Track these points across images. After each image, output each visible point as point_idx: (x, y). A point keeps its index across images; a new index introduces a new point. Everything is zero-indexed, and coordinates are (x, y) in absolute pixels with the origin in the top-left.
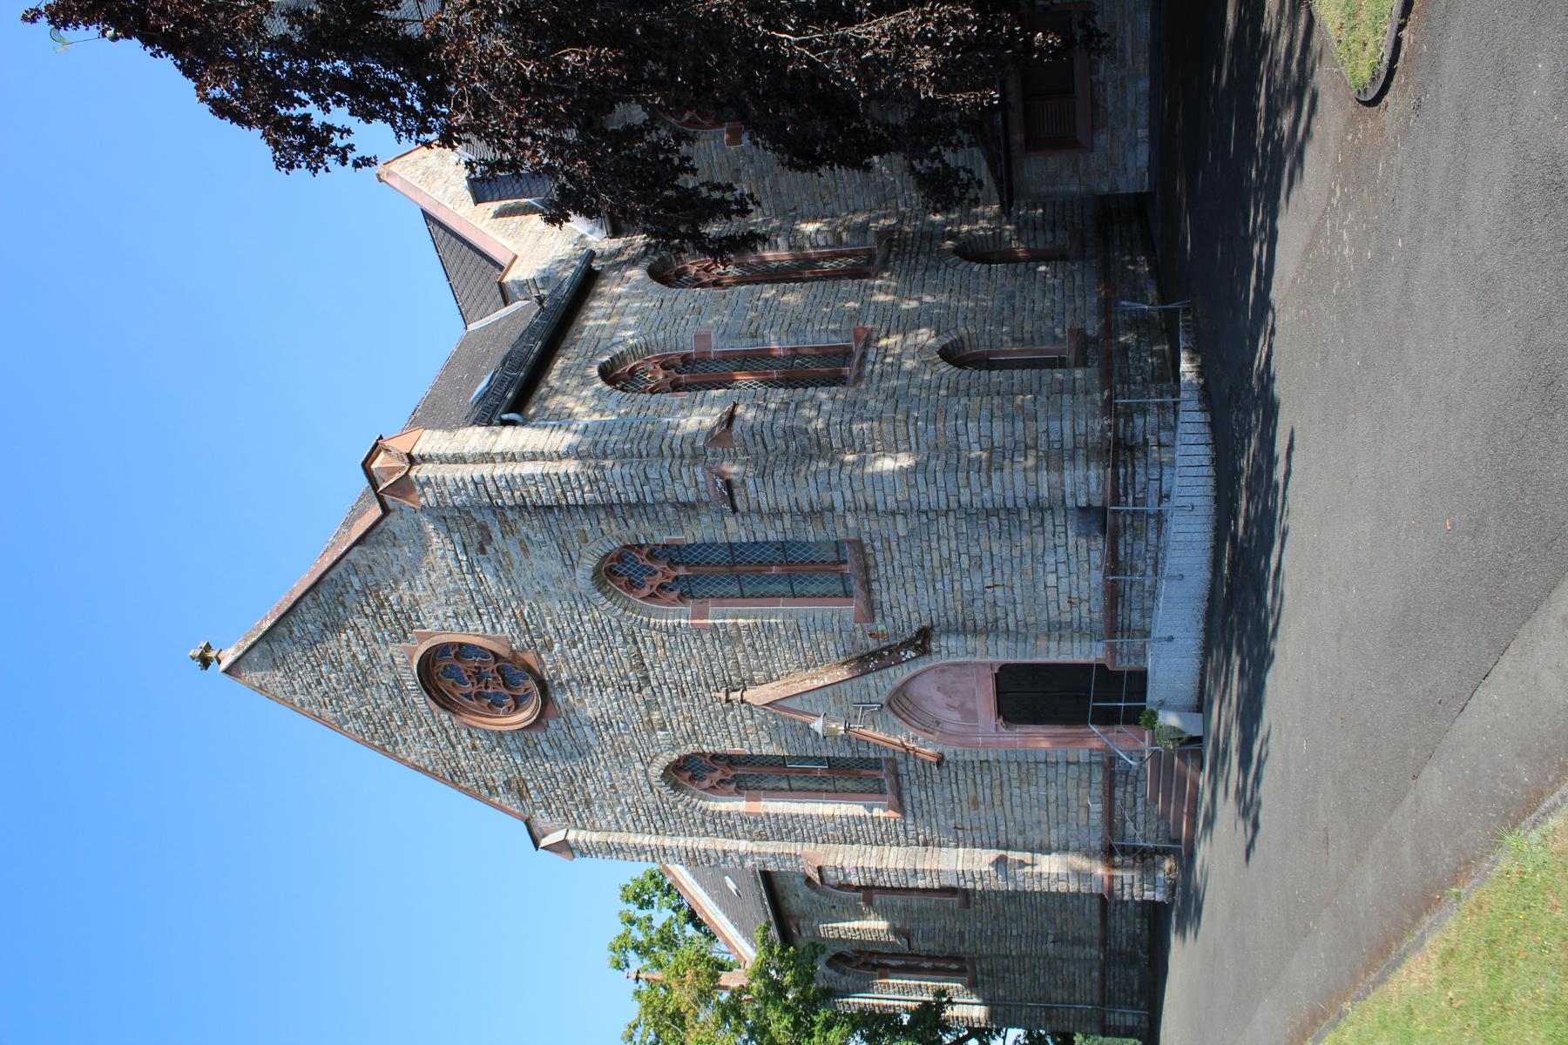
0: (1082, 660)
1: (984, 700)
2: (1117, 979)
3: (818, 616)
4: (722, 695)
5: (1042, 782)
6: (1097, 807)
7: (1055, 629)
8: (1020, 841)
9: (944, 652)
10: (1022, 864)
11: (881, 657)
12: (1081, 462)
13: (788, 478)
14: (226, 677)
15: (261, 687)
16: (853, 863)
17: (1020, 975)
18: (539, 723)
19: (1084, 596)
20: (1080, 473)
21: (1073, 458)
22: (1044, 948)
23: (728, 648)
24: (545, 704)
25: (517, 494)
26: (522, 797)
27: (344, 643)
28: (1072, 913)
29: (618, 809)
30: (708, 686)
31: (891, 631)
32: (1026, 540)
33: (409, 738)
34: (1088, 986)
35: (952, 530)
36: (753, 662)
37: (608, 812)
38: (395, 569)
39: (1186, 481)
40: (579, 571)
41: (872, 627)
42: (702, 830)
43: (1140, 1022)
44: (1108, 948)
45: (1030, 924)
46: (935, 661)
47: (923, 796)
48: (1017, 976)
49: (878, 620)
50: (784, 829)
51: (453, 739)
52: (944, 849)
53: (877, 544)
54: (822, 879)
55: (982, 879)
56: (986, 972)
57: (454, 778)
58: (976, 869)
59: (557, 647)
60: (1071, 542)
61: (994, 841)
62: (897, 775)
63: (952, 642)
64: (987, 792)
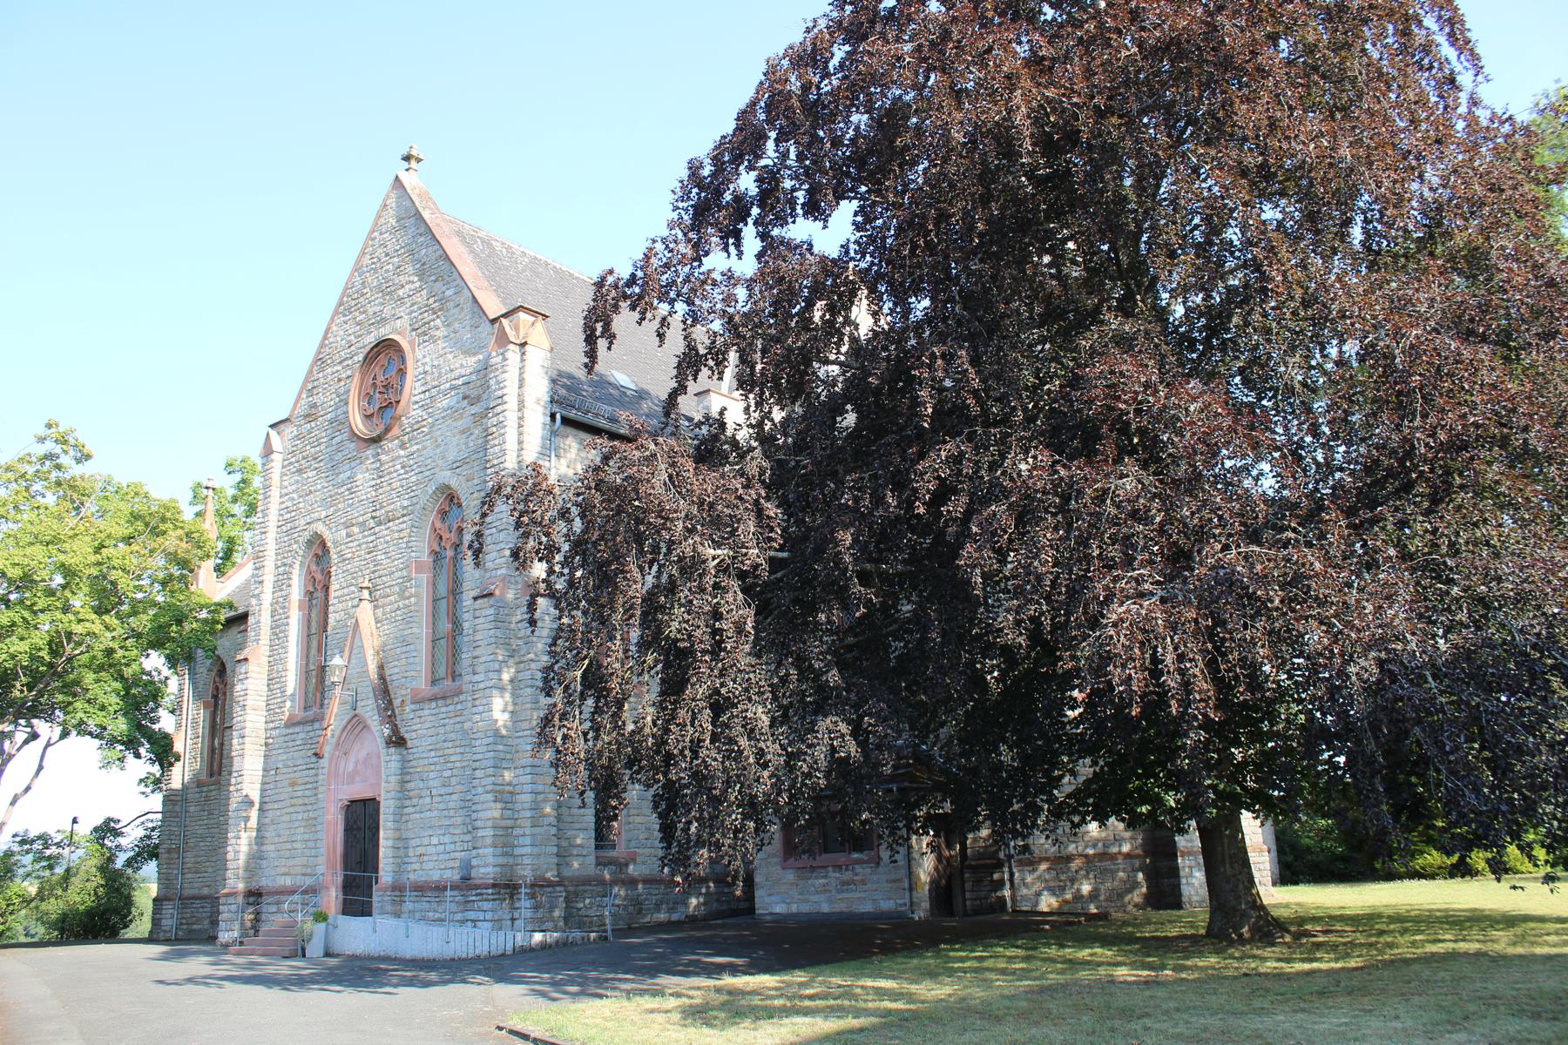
0: (381, 866)
1: (360, 791)
3: (417, 660)
4: (366, 584)
5: (306, 837)
6: (288, 881)
7: (402, 843)
8: (267, 821)
9: (388, 758)
10: (247, 819)
11: (386, 709)
12: (501, 860)
13: (493, 640)
14: (393, 178)
15: (385, 205)
16: (250, 687)
18: (354, 436)
19: (425, 866)
20: (491, 860)
21: (504, 854)
23: (397, 588)
24: (365, 440)
25: (494, 429)
26: (306, 416)
27: (412, 278)
29: (295, 496)
30: (374, 572)
31: (405, 716)
32: (459, 820)
33: (347, 327)
34: (196, 885)
36: (388, 609)
37: (294, 487)
38: (457, 325)
39: (465, 936)
40: (449, 473)
41: (408, 702)
42: (279, 563)
46: (383, 751)
47: (298, 743)
49: (413, 707)
50: (278, 629)
51: (346, 363)
52: (262, 759)
53: (459, 707)
54: (239, 661)
55: (237, 790)
57: (319, 361)
58: (244, 786)
59: (402, 453)
60: (458, 855)
61: (267, 799)
62: (312, 721)
63: (394, 765)
64: (300, 793)
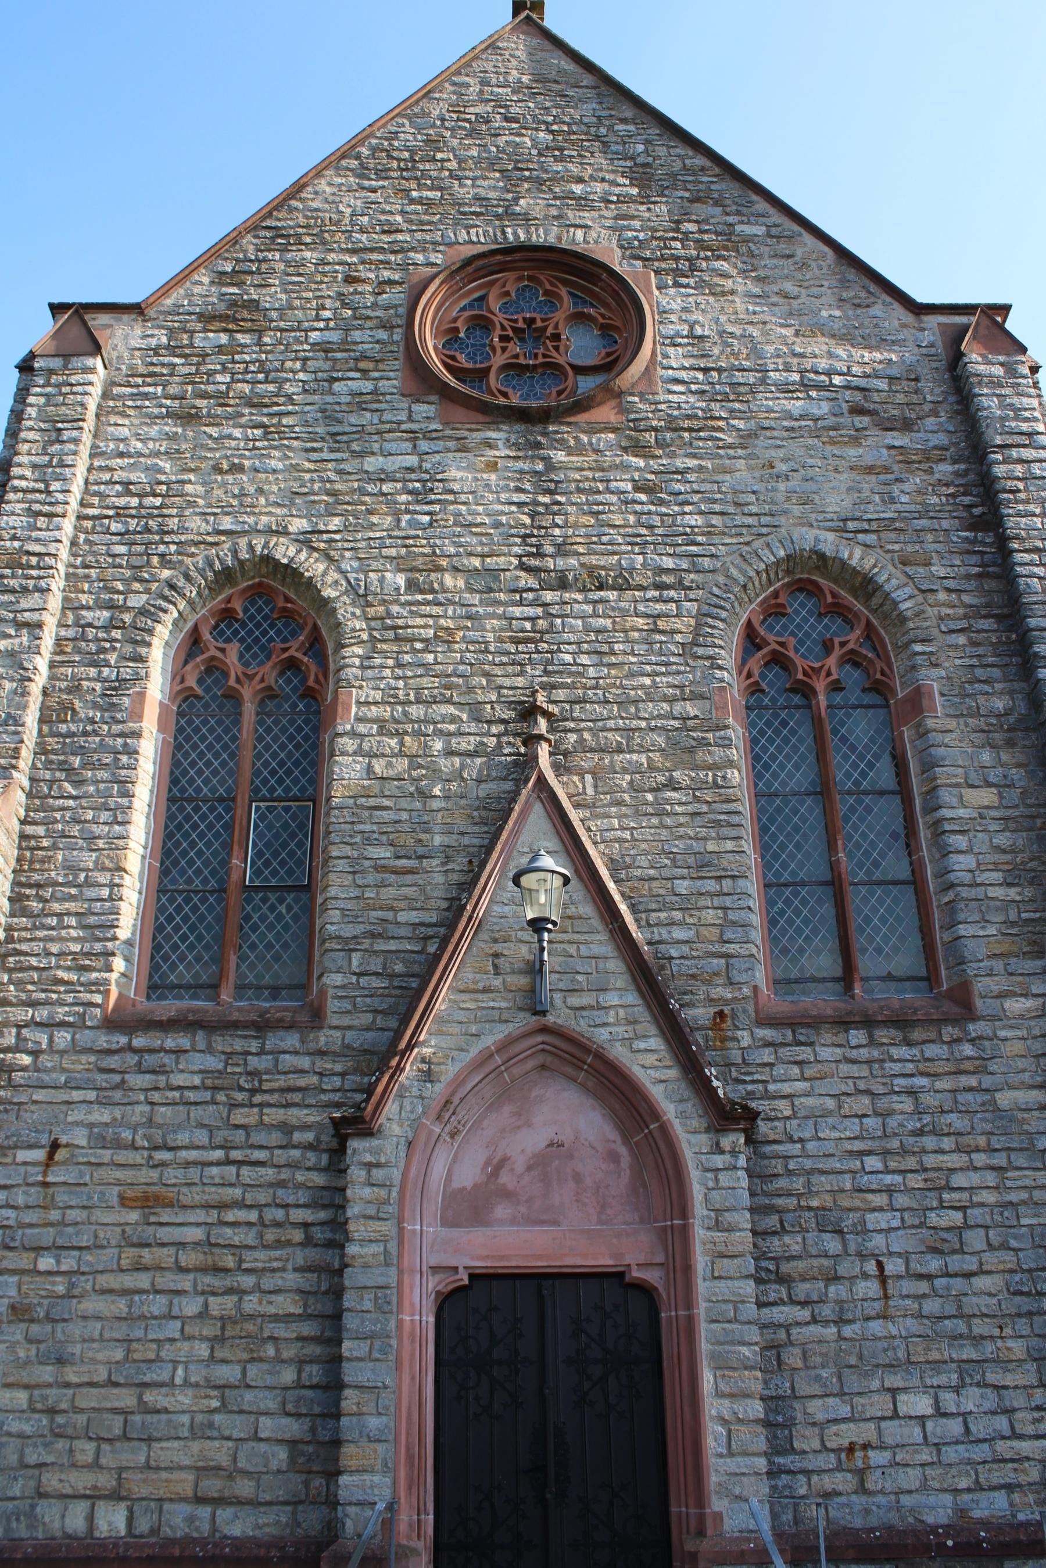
9: (719, 1161)
32: (1017, 1348)
35: (1024, 1195)
41: (743, 1020)
60: (1025, 1447)
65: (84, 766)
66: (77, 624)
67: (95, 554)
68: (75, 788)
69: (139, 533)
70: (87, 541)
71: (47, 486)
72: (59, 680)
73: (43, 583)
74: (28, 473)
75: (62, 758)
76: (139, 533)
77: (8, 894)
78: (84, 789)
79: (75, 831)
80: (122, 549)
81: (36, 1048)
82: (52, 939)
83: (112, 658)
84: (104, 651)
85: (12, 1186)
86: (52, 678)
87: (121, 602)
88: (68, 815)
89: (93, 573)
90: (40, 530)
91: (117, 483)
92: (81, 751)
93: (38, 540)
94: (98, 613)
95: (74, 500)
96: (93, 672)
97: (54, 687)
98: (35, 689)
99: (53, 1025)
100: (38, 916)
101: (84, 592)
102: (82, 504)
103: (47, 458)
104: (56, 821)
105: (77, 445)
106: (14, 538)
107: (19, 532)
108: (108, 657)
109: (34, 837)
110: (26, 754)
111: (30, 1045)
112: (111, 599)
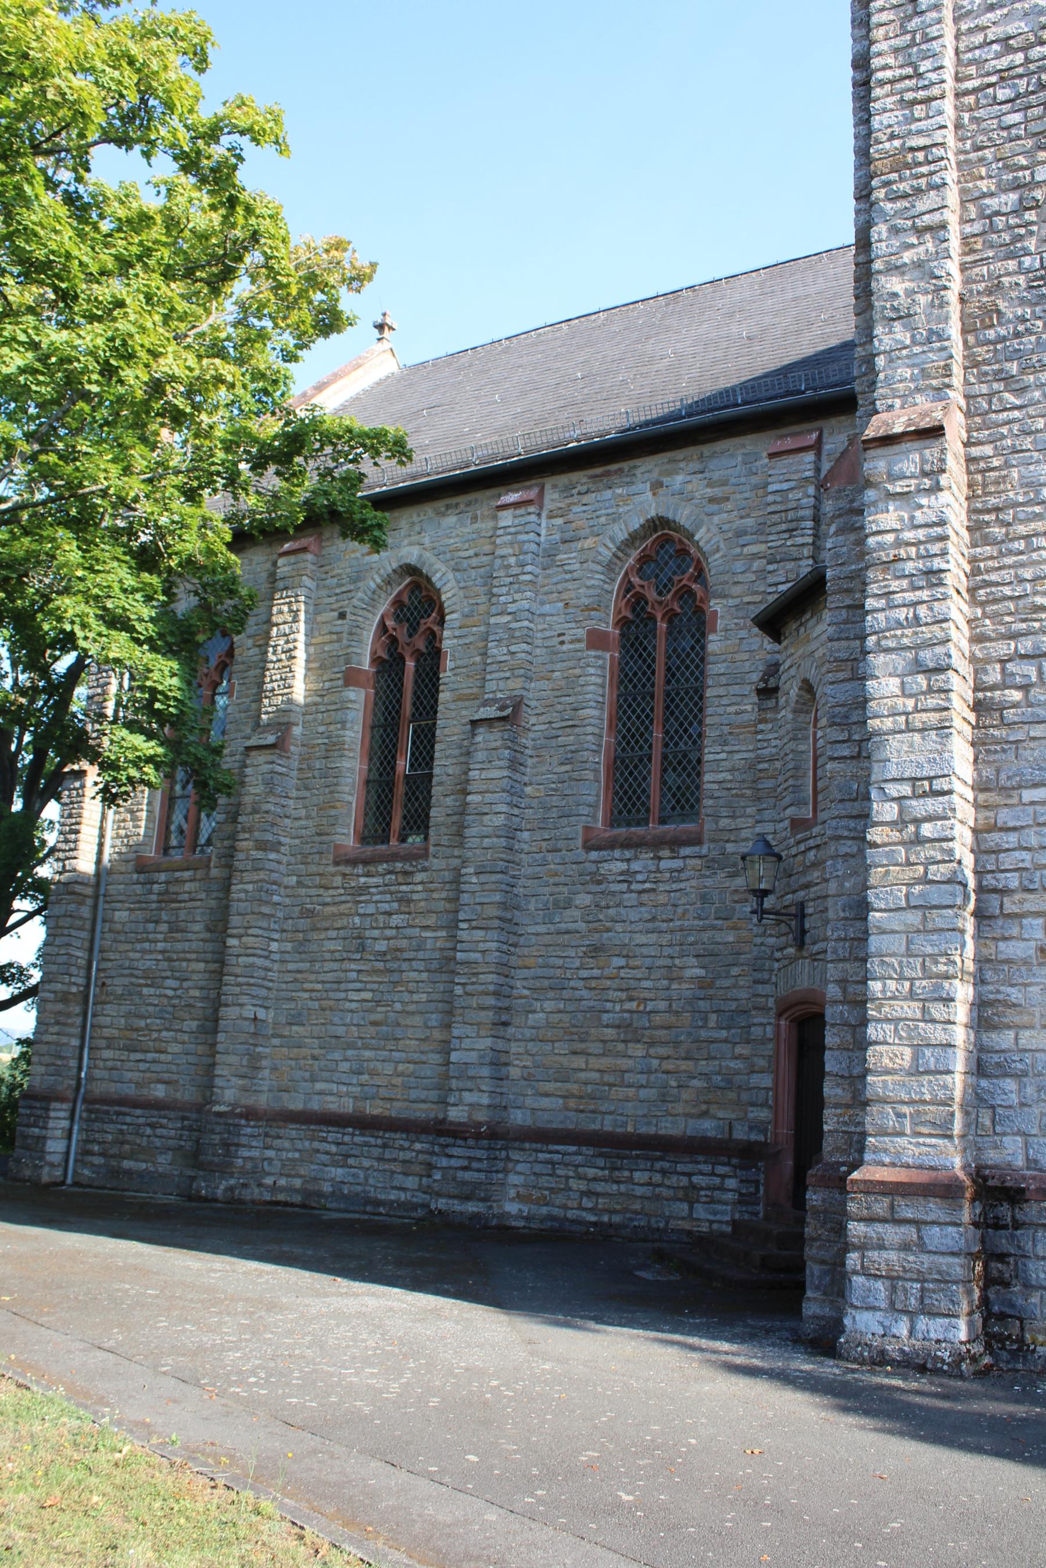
2: (148, 1131)
17: (162, 952)
22: (244, 999)
28: (314, 1058)
43: (52, 1165)
44: (243, 1122)
45: (289, 977)
48: (160, 946)
56: (173, 889)
65: (1023, 371)
66: (982, 216)
67: (985, 132)
68: (1017, 397)
69: (1033, 93)
70: (974, 120)
71: (916, 68)
72: (975, 282)
73: (936, 179)
74: (890, 60)
75: (996, 367)
76: (1033, 93)
77: (966, 523)
78: (1028, 396)
79: (1027, 443)
80: (1017, 117)
81: (1024, 682)
82: (1023, 565)
83: (1031, 244)
84: (1020, 238)
85: (1022, 827)
86: (967, 282)
87: (1028, 179)
88: (1016, 428)
89: (988, 154)
90: (920, 120)
91: (993, 42)
92: (1017, 355)
93: (919, 132)
94: (1003, 198)
95: (948, 75)
96: (1012, 265)
97: (971, 291)
98: (952, 296)
99: (1040, 656)
100: (1003, 541)
101: (982, 178)
102: (958, 79)
103: (908, 37)
104: (1003, 437)
105: (939, 11)
106: (892, 137)
107: (896, 129)
108: (1026, 244)
109: (982, 458)
110: (957, 370)
111: (1018, 679)
112: (1016, 178)
